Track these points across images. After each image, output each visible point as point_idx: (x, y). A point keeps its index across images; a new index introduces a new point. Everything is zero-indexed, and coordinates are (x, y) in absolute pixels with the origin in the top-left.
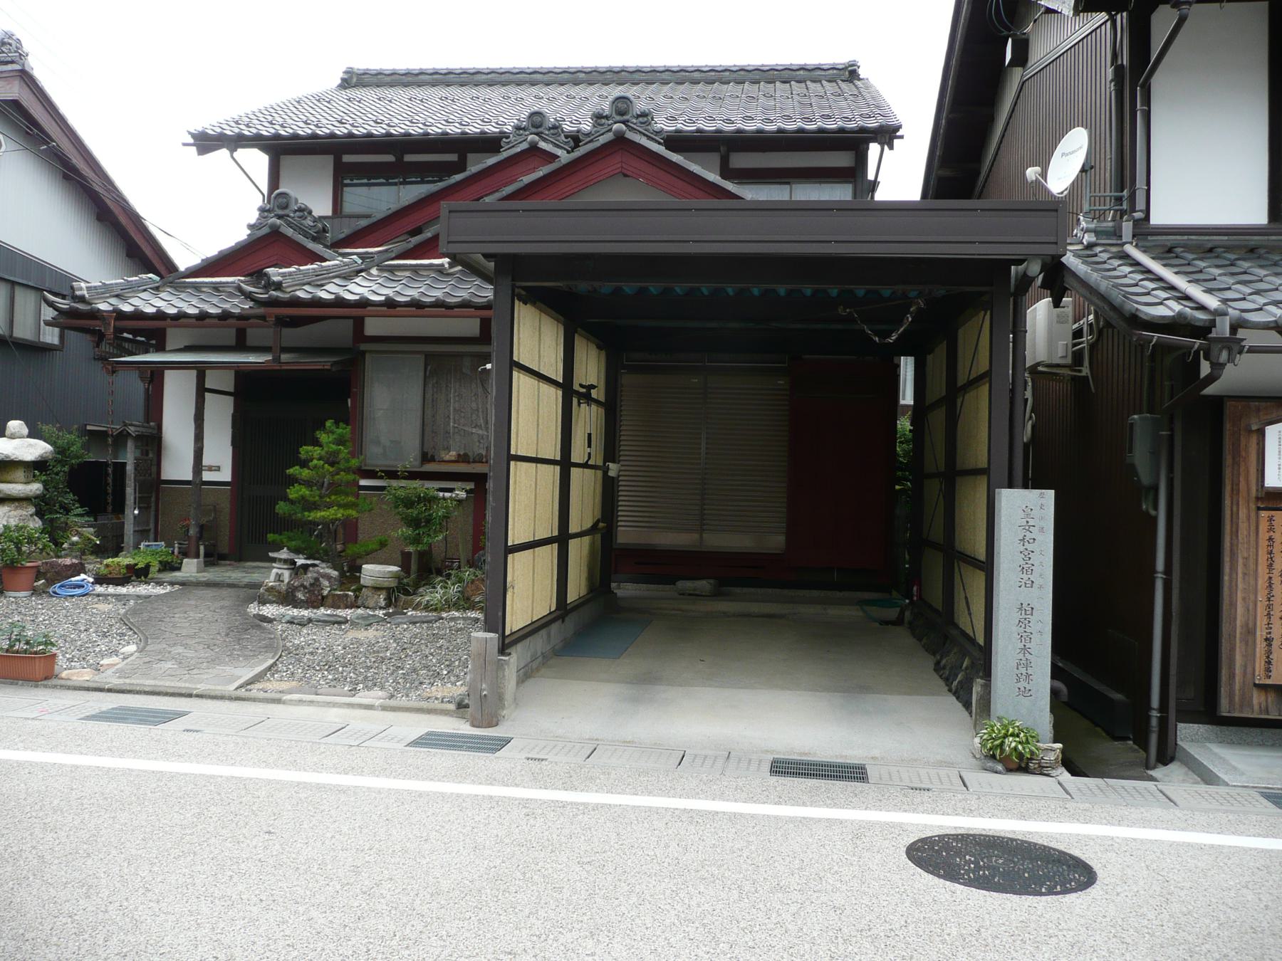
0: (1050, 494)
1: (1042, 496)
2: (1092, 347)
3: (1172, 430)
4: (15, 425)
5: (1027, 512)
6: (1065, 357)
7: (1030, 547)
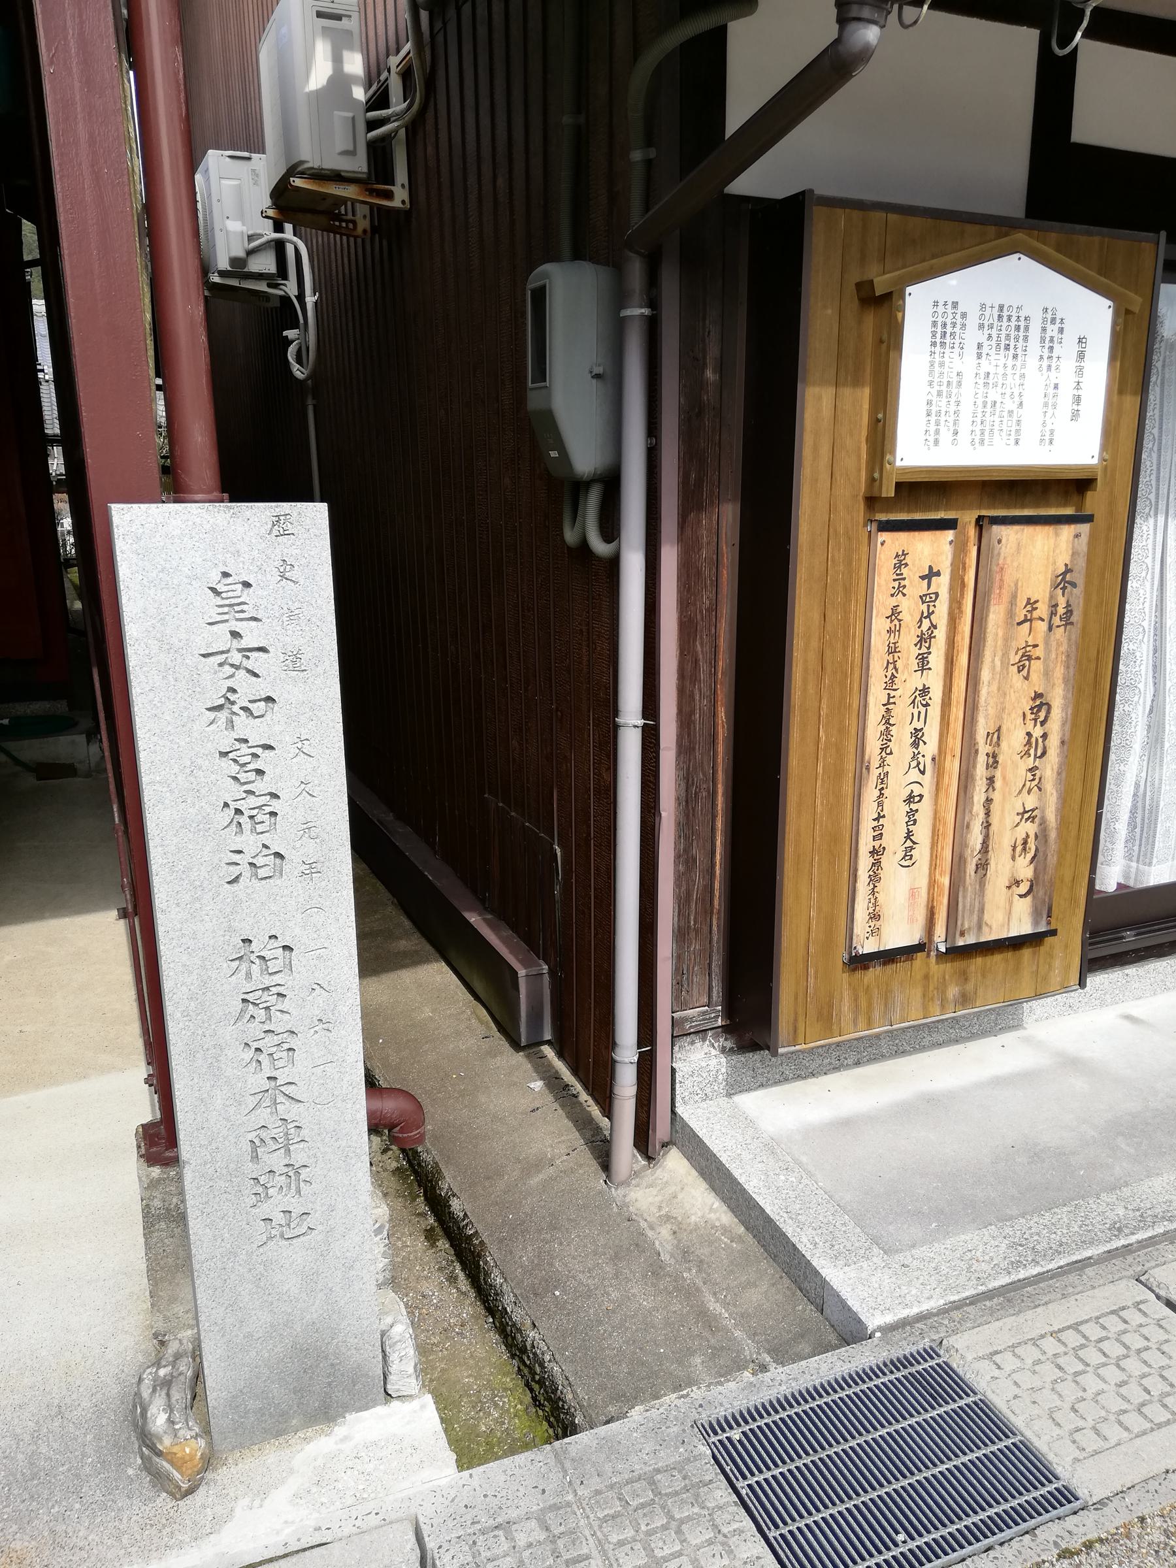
0: (312, 519)
1: (279, 527)
2: (414, 128)
3: (653, 303)
4: (570, 536)
5: (229, 593)
6: (351, 153)
7: (255, 731)
